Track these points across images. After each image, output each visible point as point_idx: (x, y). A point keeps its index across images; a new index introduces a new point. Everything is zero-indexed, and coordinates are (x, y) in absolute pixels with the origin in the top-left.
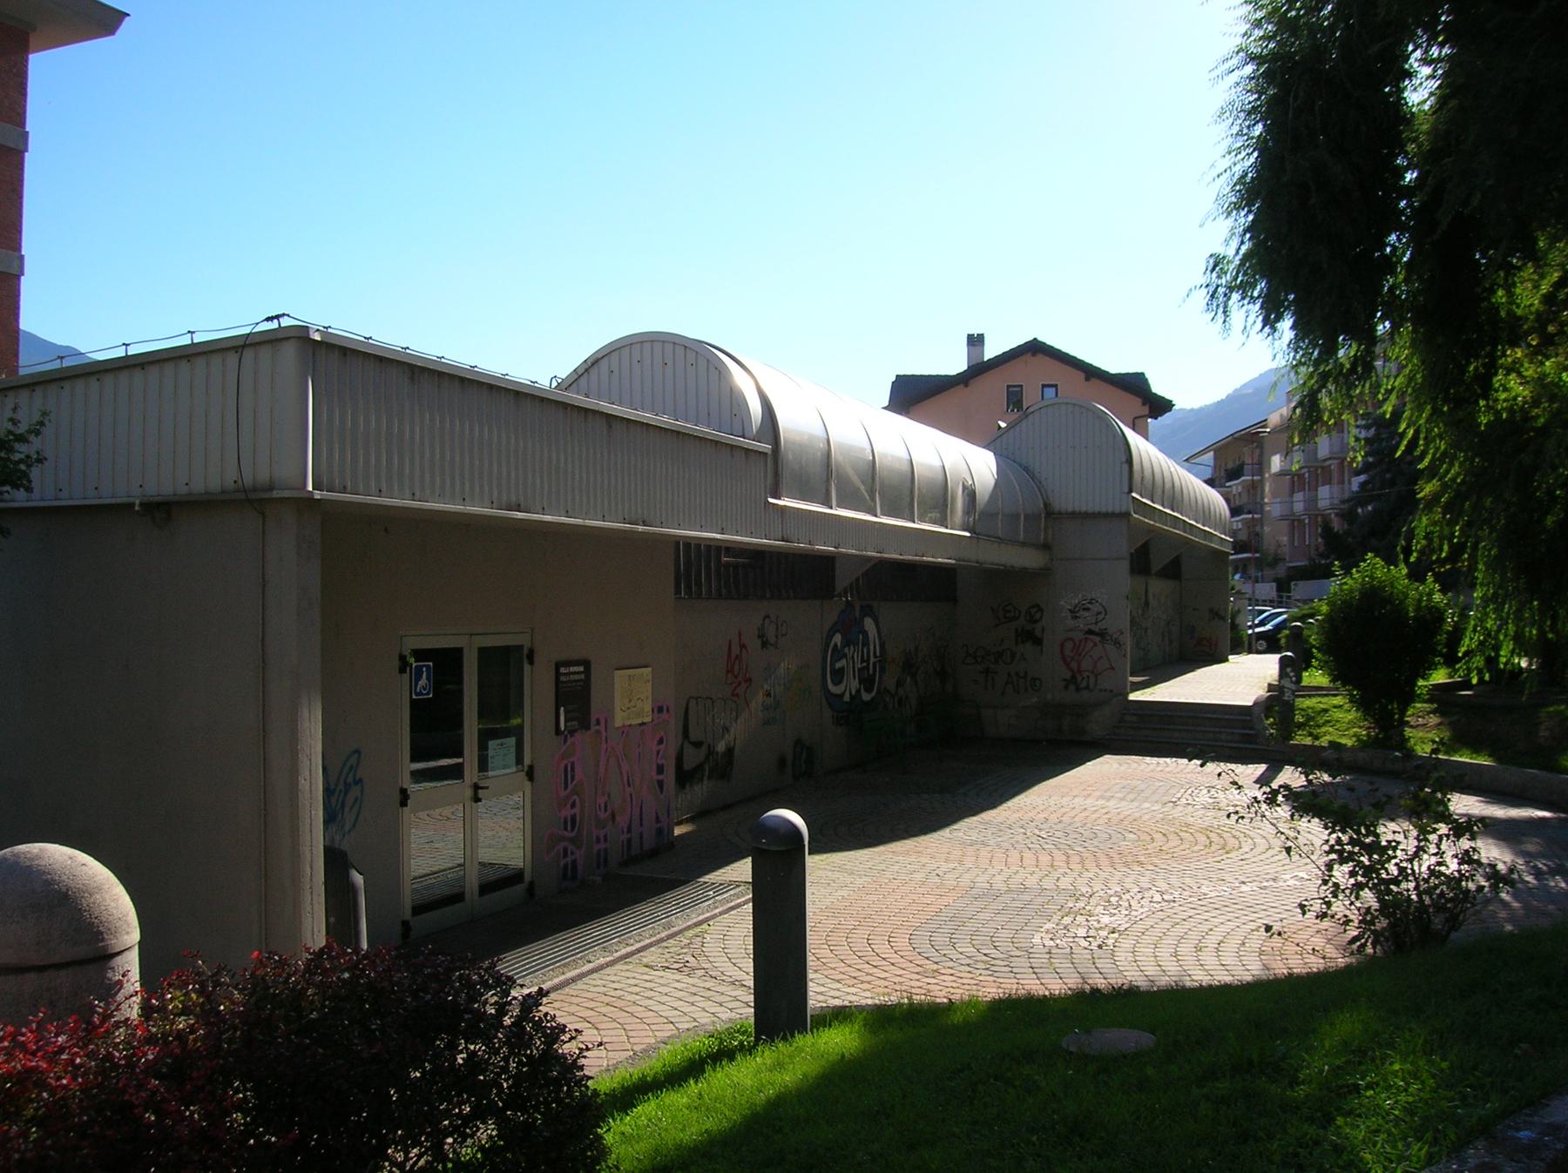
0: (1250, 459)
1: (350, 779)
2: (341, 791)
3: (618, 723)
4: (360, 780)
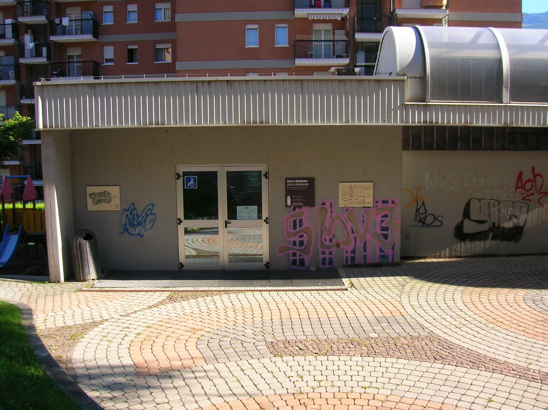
0: (332, 36)
1: (149, 212)
2: (144, 216)
3: (341, 204)
4: (154, 214)
